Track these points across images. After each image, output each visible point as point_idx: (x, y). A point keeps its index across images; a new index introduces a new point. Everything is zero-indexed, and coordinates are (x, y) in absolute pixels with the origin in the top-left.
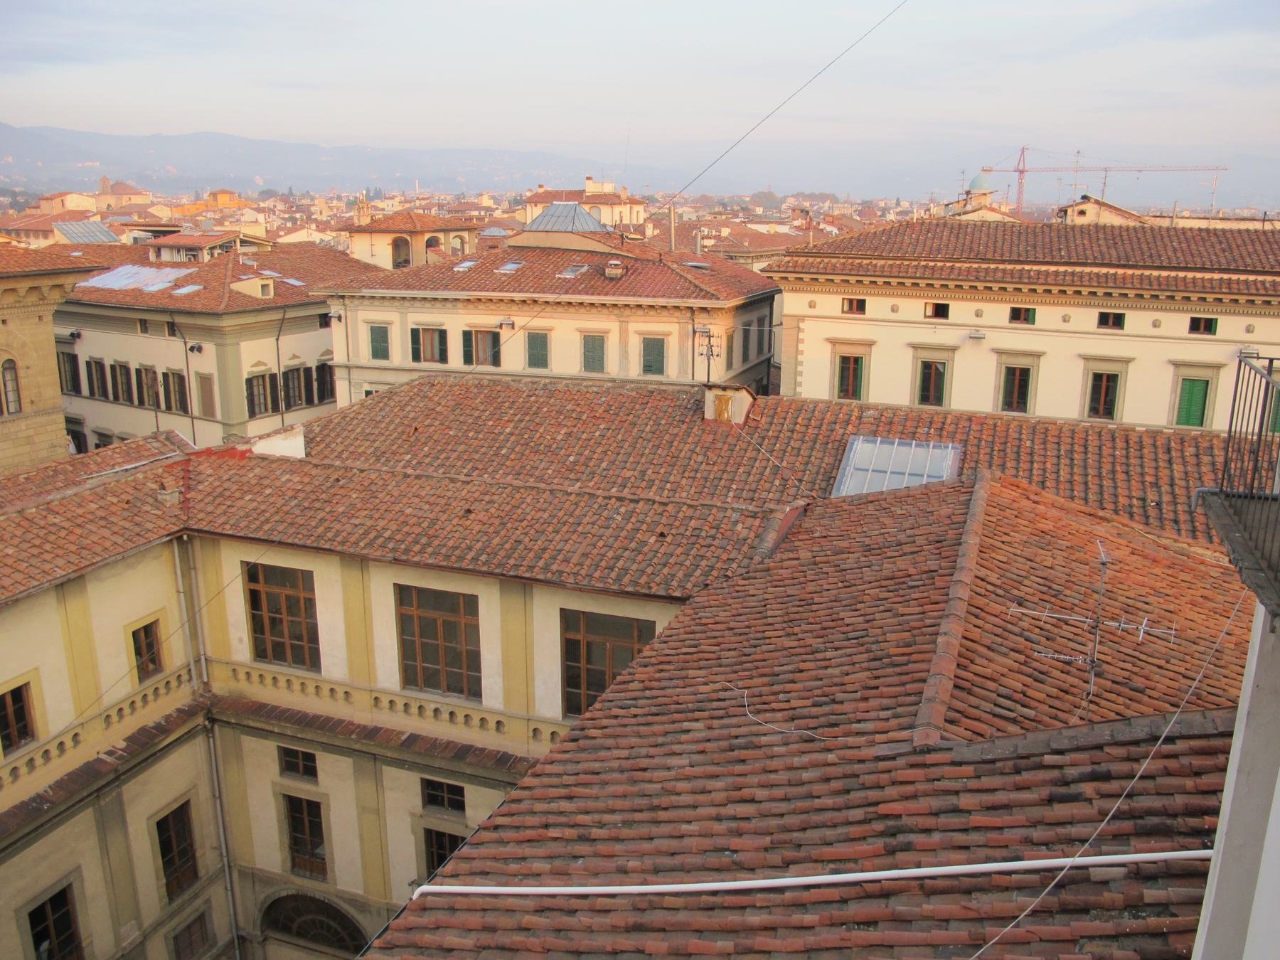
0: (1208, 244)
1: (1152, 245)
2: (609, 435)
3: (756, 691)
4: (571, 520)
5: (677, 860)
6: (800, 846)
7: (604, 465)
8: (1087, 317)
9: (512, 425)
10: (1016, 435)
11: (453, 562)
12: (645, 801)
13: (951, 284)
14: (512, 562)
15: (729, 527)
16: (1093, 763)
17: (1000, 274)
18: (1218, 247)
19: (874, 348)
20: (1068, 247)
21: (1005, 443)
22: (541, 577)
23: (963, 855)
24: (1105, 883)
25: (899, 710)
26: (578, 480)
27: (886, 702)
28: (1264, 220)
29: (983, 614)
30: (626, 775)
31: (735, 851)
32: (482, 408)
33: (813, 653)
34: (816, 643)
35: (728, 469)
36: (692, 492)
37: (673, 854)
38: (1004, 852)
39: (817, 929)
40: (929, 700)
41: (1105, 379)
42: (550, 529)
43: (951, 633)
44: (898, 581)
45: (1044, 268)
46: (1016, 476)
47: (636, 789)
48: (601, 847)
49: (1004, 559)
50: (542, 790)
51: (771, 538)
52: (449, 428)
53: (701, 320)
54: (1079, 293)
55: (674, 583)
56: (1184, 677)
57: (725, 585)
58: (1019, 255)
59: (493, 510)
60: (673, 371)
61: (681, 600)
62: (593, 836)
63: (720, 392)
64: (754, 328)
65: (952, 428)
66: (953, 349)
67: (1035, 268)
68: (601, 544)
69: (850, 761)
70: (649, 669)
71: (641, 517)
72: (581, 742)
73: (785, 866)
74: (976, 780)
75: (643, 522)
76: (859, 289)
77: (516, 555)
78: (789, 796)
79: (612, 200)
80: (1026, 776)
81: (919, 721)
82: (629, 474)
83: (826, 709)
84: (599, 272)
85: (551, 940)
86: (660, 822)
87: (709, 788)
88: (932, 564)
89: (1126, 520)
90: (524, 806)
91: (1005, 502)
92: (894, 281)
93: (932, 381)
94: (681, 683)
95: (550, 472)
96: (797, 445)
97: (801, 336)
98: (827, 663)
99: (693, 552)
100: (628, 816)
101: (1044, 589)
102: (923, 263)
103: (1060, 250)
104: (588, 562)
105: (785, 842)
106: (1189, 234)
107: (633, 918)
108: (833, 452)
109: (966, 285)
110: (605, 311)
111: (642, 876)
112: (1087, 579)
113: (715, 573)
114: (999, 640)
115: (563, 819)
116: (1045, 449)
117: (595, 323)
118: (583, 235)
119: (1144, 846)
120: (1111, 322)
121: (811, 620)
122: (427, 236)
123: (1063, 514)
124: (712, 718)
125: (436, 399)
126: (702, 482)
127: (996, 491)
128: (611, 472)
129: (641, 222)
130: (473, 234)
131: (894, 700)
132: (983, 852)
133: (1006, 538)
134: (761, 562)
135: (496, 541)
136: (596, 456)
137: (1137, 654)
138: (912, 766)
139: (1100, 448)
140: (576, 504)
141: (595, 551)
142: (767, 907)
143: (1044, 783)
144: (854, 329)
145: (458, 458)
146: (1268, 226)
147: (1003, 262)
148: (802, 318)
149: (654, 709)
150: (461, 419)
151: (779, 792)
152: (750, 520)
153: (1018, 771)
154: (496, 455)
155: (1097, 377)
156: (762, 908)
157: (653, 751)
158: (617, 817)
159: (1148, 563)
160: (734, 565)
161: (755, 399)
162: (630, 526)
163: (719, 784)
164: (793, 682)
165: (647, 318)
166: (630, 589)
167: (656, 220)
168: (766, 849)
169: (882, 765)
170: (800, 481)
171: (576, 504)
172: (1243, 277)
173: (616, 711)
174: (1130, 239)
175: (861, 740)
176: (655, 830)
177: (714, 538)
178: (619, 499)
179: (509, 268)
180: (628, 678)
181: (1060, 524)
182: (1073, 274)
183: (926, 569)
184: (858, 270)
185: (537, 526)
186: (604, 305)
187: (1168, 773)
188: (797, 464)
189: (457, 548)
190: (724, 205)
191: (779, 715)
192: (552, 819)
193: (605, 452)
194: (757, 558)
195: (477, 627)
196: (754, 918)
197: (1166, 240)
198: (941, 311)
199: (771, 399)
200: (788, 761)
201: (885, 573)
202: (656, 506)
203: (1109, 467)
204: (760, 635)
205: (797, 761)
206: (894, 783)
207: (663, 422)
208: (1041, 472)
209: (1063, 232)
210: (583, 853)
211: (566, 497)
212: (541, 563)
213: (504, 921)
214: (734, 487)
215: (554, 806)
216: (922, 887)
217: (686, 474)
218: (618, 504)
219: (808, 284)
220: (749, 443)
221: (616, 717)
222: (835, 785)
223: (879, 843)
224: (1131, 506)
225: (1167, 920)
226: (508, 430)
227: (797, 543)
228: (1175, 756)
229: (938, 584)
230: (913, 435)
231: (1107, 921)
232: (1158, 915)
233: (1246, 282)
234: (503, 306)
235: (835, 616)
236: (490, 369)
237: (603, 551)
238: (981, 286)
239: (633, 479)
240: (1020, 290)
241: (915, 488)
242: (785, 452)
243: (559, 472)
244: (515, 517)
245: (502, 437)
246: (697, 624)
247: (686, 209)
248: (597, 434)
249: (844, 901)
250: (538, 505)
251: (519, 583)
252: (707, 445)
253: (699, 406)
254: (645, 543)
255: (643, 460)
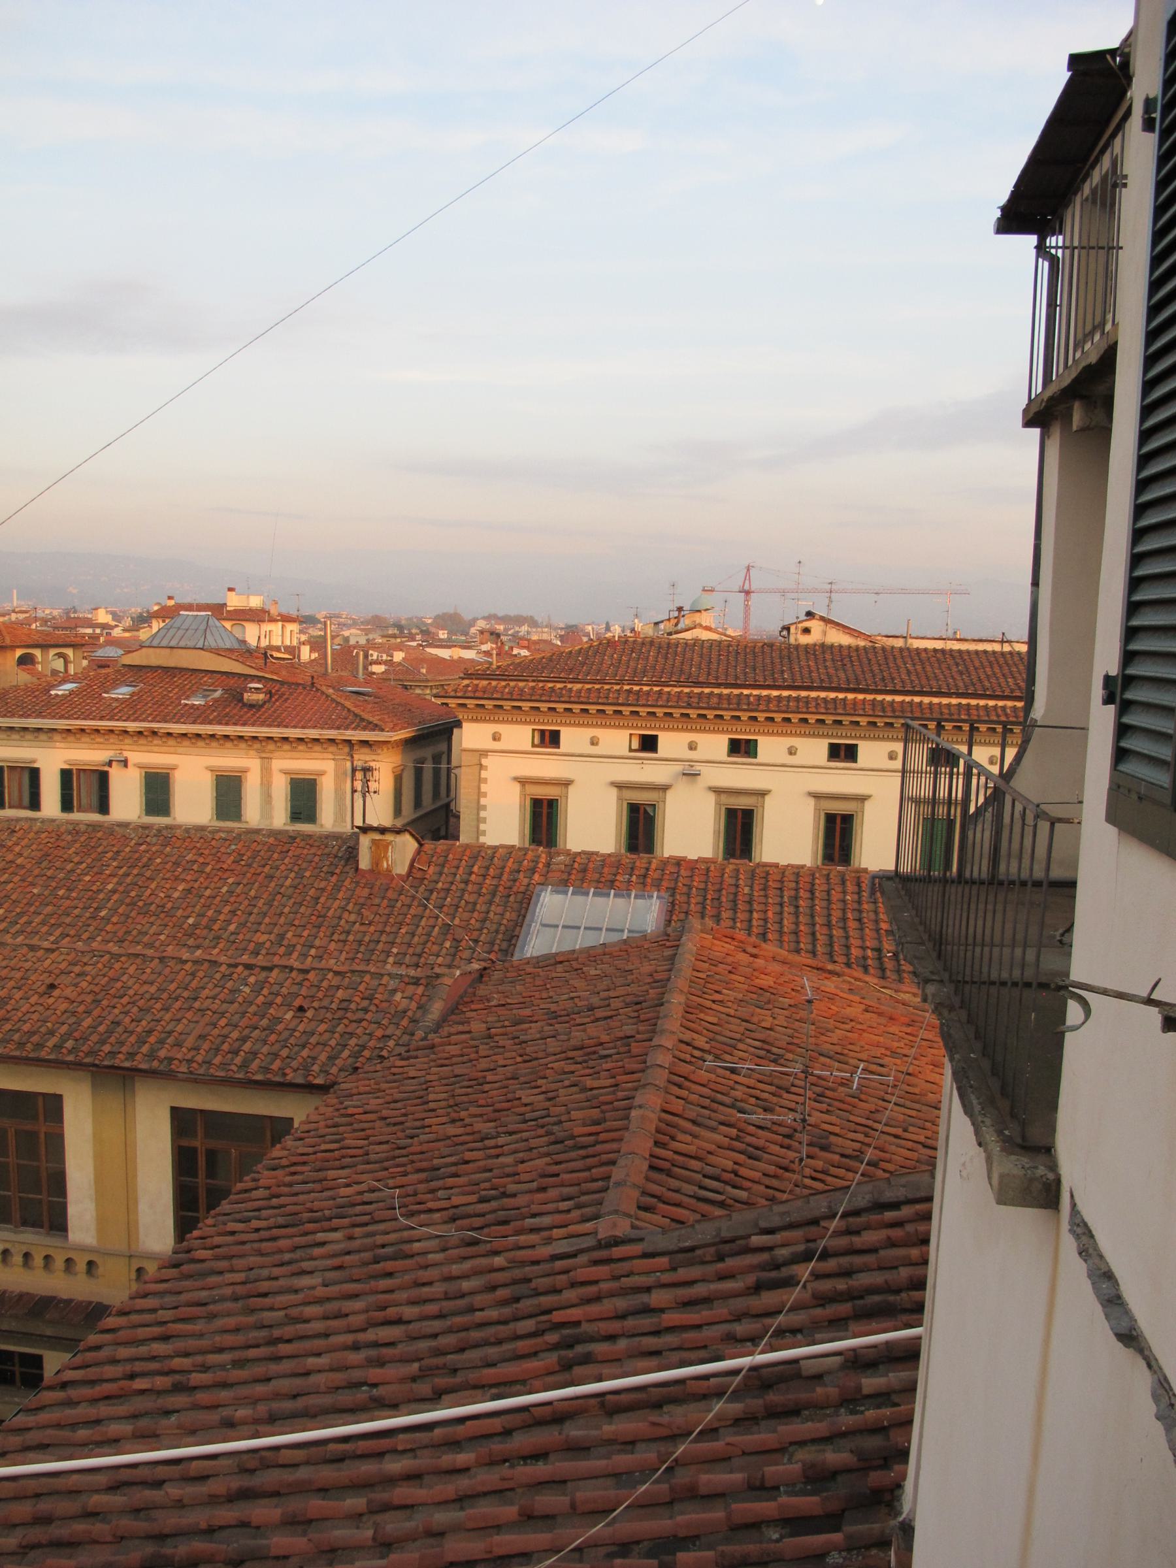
0: (944, 666)
1: (884, 667)
2: (238, 890)
3: (410, 1189)
4: (186, 994)
5: (300, 1403)
6: (456, 1370)
7: (232, 928)
8: (815, 749)
9: (115, 880)
10: (732, 881)
11: (29, 1051)
12: (263, 1333)
13: (660, 712)
14: (107, 1048)
15: (386, 996)
16: (808, 1241)
17: (715, 700)
18: (954, 669)
19: (571, 788)
20: (791, 669)
21: (720, 890)
22: (143, 1066)
23: (654, 1362)
24: (818, 1377)
25: (584, 1198)
26: (198, 947)
27: (566, 1191)
28: (1002, 642)
29: (687, 1084)
30: (240, 1304)
31: (375, 1385)
32: (76, 859)
33: (482, 1140)
34: (486, 1127)
35: (388, 929)
36: (342, 958)
37: (295, 1397)
38: (702, 1354)
39: (473, 1471)
40: (618, 1184)
41: (838, 821)
42: (158, 1006)
43: (648, 1106)
44: (589, 1052)
45: (765, 693)
46: (733, 928)
47: (251, 1319)
48: (202, 1397)
49: (715, 1020)
50: (129, 1331)
51: (437, 1009)
52: (33, 884)
53: (362, 757)
54: (805, 721)
55: (316, 1068)
56: (925, 1146)
57: (379, 1067)
58: (737, 678)
59: (84, 984)
60: (329, 818)
61: (324, 1089)
62: (192, 1383)
63: (377, 836)
64: (428, 766)
65: (656, 875)
66: (664, 788)
67: (755, 692)
68: (223, 1022)
69: (523, 1263)
70: (279, 1172)
71: (276, 988)
72: (185, 1268)
73: (436, 1398)
74: (672, 1273)
75: (277, 994)
76: (551, 717)
77: (112, 1040)
78: (444, 1312)
79: (258, 616)
80: (730, 1262)
81: (605, 1209)
82: (264, 938)
83: (494, 1204)
84: (235, 697)
85: (126, 1523)
86: (281, 1358)
87: (345, 1310)
88: (629, 1029)
89: (858, 973)
90: (104, 1353)
91: (717, 955)
92: (593, 708)
93: (641, 824)
94: (317, 1186)
95: (162, 937)
96: (472, 898)
97: (484, 774)
98: (498, 1151)
99: (340, 1028)
100: (237, 1355)
101: (762, 1053)
102: (626, 687)
103: (782, 672)
104: (206, 1046)
105: (438, 1368)
106: (924, 655)
107: (236, 1483)
108: (515, 906)
109: (677, 713)
110: (243, 745)
111: (253, 1427)
112: (812, 1040)
113: (367, 1053)
114: (706, 1112)
115: (154, 1366)
116: (766, 896)
117: (230, 760)
118: (217, 652)
119: (863, 1328)
120: (842, 754)
121: (481, 1102)
122: (19, 653)
123: (785, 968)
124: (354, 1226)
125: (17, 849)
126: (355, 946)
127: (707, 944)
128: (241, 937)
129: (295, 643)
130: (79, 653)
131: (576, 1188)
132: (676, 1356)
133: (717, 997)
134: (425, 1039)
135: (87, 1022)
136: (222, 917)
137: (870, 1123)
138: (596, 1263)
139: (828, 892)
140: (193, 974)
141: (216, 1032)
142: (412, 1450)
143: (752, 1268)
144: (546, 766)
145: (43, 923)
146: (1007, 648)
147: (719, 685)
148: (484, 753)
149: (281, 1220)
150: (49, 873)
151: (432, 1308)
152: (412, 987)
153: (721, 1258)
154: (93, 918)
155: (830, 819)
156: (404, 1451)
157: (276, 1271)
158: (226, 1357)
159: (883, 1020)
160: (391, 1043)
161: (421, 845)
162: (261, 998)
163: (359, 1305)
164: (456, 1175)
165: (295, 754)
166: (259, 1077)
167: (317, 644)
168: (414, 1379)
169: (559, 1264)
170: (476, 941)
171: (193, 974)
172: (982, 703)
173: (232, 1226)
174: (860, 661)
175: (533, 1238)
176: (274, 1368)
177: (366, 1010)
178: (248, 967)
179: (123, 692)
180: (251, 1185)
181: (781, 980)
182: (797, 699)
183: (621, 1034)
184: (551, 696)
185: (141, 1003)
186: (241, 737)
187: (892, 1244)
188: (473, 921)
189: (34, 1033)
190: (400, 627)
191: (437, 1216)
192: (139, 1366)
193: (233, 912)
194: (420, 1034)
195: (60, 1137)
196: (394, 1466)
197: (899, 661)
198: (649, 744)
199: (442, 845)
200: (445, 1270)
201: (573, 1042)
202: (294, 974)
203: (839, 914)
204: (418, 1124)
205: (455, 1269)
206: (573, 1285)
207: (307, 874)
208: (761, 923)
209: (785, 653)
210: (177, 1407)
211: (179, 967)
212: (145, 1049)
213: (64, 1506)
214: (395, 950)
215: (143, 1350)
216: (602, 1405)
217: (335, 937)
218: (246, 973)
219: (490, 712)
220: (414, 897)
221: (233, 1233)
222: (502, 1293)
223: (551, 1359)
224: (865, 958)
225: (887, 1411)
226: (110, 887)
227: (469, 1014)
228: (898, 1224)
229: (635, 1051)
230: (612, 884)
231: (820, 1421)
232: (878, 1407)
233: (986, 707)
234: (113, 739)
235: (510, 1096)
236: (96, 817)
237: (225, 1031)
238: (695, 715)
239: (268, 945)
240: (738, 718)
241: (614, 945)
242: (457, 907)
243: (174, 937)
244: (112, 992)
245: (101, 896)
246: (343, 1115)
247: (353, 631)
248: (225, 889)
249: (507, 1433)
250: (144, 977)
251: (116, 1076)
252: (361, 901)
253: (352, 854)
254: (278, 1020)
255: (282, 920)
